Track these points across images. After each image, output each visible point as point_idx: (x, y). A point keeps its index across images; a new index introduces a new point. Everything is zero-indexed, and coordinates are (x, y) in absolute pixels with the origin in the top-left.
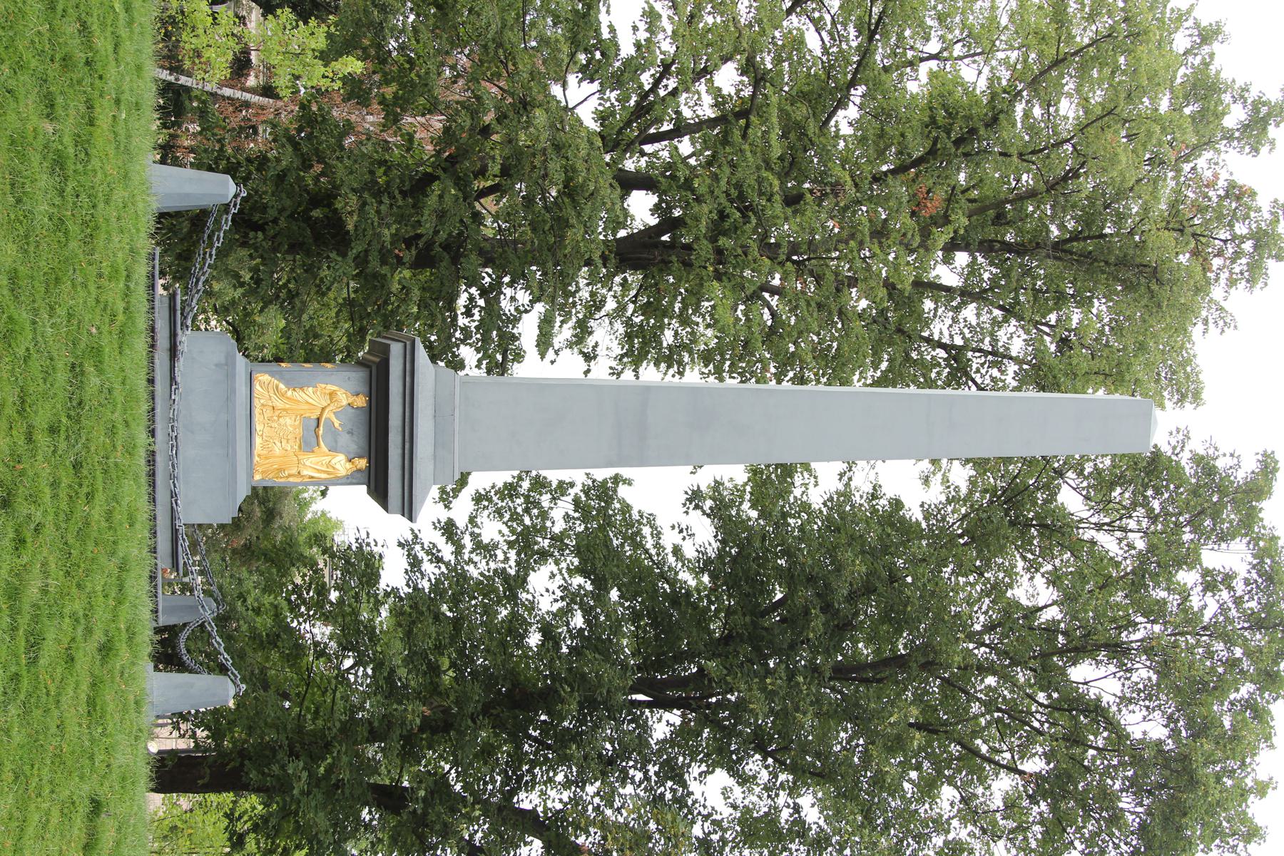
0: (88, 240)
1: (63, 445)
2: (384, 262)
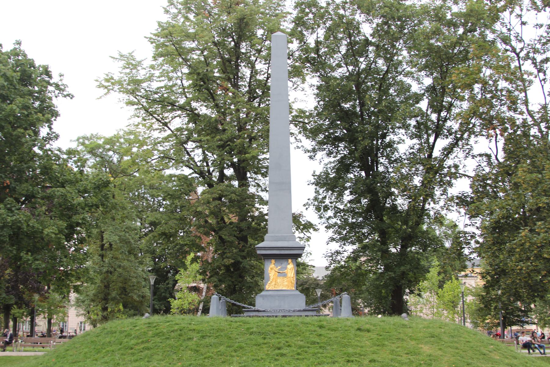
0: (222, 330)
1: (269, 336)
2: (243, 251)
